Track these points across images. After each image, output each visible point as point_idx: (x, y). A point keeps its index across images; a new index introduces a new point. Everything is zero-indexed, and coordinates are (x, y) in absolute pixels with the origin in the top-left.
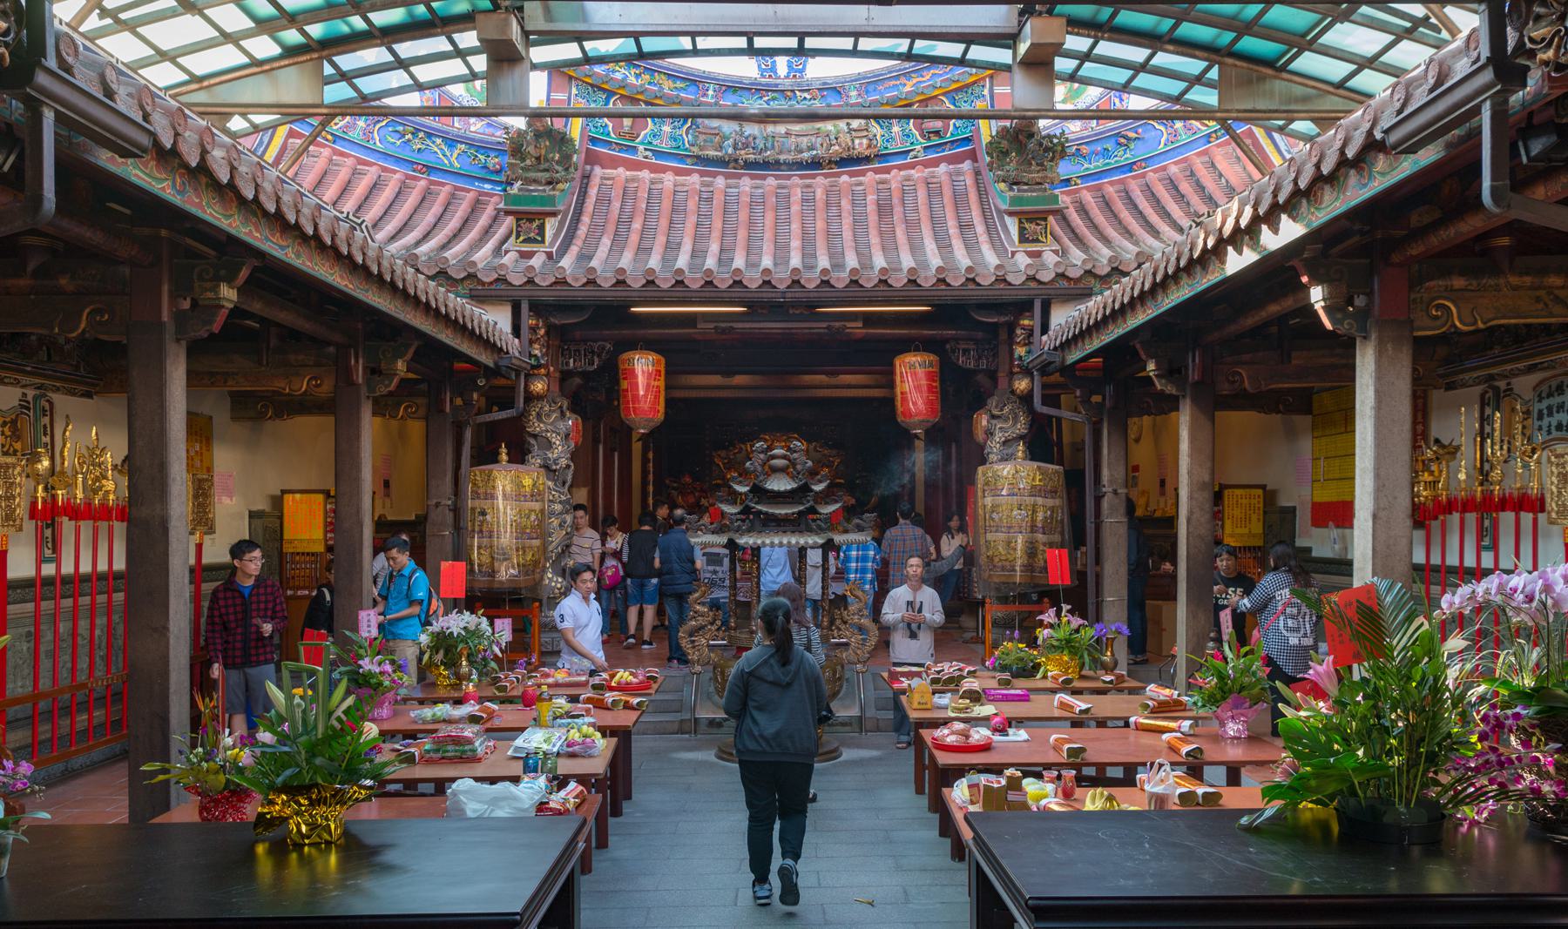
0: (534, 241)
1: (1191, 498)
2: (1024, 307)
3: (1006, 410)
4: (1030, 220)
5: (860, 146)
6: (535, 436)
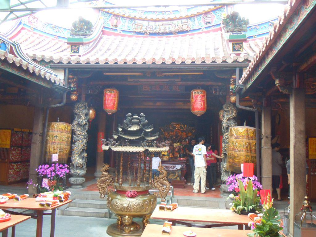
0: (76, 52)
1: (295, 137)
2: (233, 71)
3: (229, 108)
4: (236, 44)
5: (185, 28)
6: (76, 114)
